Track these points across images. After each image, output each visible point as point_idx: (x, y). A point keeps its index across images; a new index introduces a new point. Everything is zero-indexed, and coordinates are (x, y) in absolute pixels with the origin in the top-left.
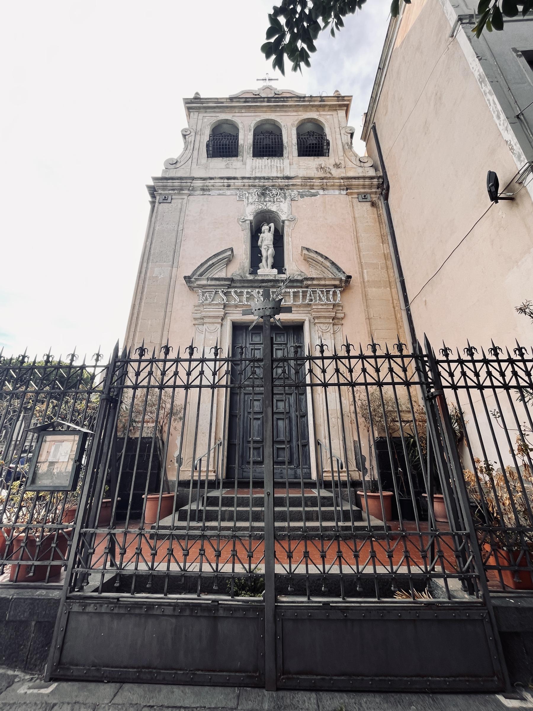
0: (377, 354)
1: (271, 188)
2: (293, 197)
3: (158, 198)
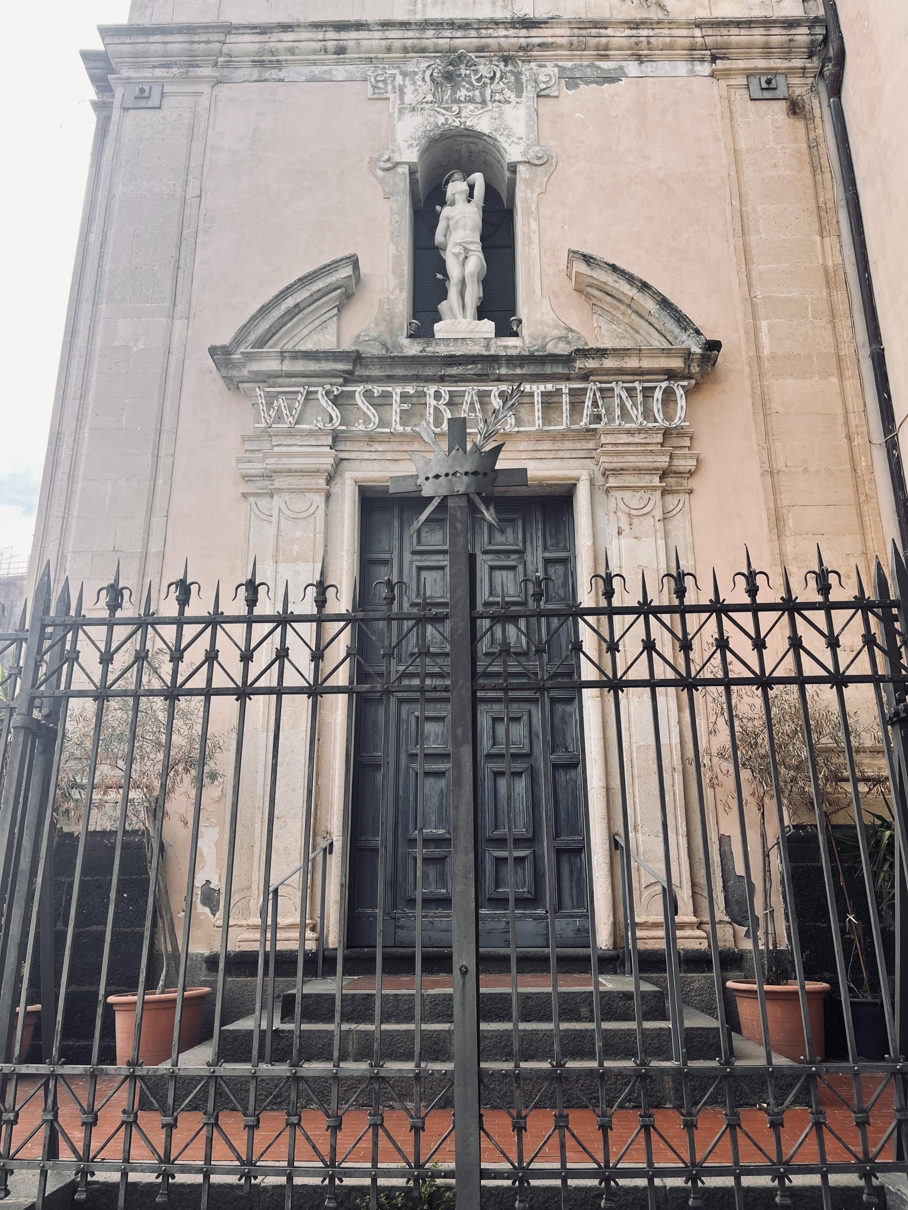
0: (760, 599)
1: (472, 55)
2: (543, 86)
3: (119, 92)
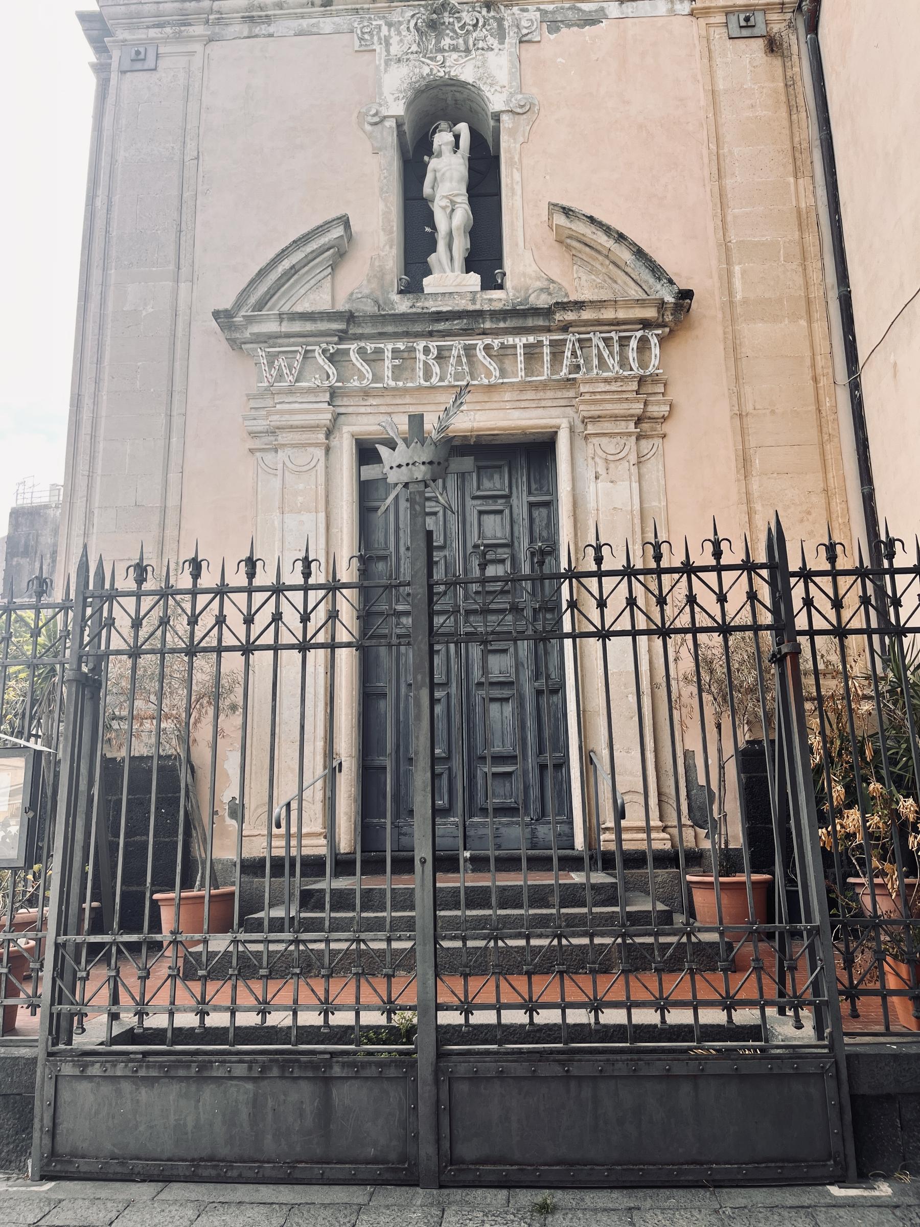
2: (525, 31)
3: (116, 54)
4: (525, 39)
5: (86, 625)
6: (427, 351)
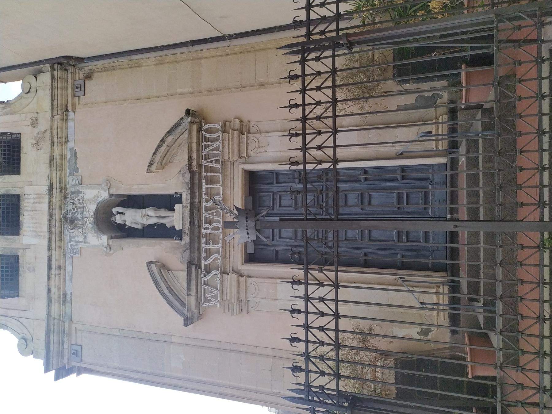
2: (77, 182)
3: (74, 364)
4: (80, 183)
5: (323, 401)
6: (207, 229)
